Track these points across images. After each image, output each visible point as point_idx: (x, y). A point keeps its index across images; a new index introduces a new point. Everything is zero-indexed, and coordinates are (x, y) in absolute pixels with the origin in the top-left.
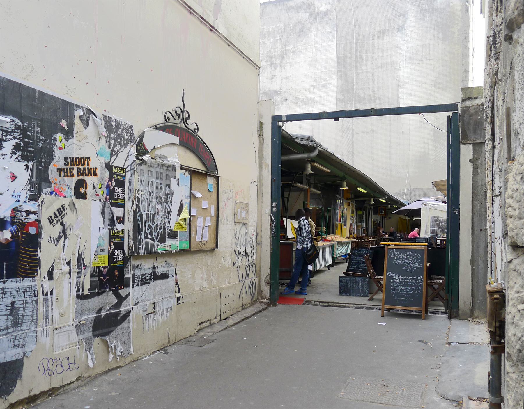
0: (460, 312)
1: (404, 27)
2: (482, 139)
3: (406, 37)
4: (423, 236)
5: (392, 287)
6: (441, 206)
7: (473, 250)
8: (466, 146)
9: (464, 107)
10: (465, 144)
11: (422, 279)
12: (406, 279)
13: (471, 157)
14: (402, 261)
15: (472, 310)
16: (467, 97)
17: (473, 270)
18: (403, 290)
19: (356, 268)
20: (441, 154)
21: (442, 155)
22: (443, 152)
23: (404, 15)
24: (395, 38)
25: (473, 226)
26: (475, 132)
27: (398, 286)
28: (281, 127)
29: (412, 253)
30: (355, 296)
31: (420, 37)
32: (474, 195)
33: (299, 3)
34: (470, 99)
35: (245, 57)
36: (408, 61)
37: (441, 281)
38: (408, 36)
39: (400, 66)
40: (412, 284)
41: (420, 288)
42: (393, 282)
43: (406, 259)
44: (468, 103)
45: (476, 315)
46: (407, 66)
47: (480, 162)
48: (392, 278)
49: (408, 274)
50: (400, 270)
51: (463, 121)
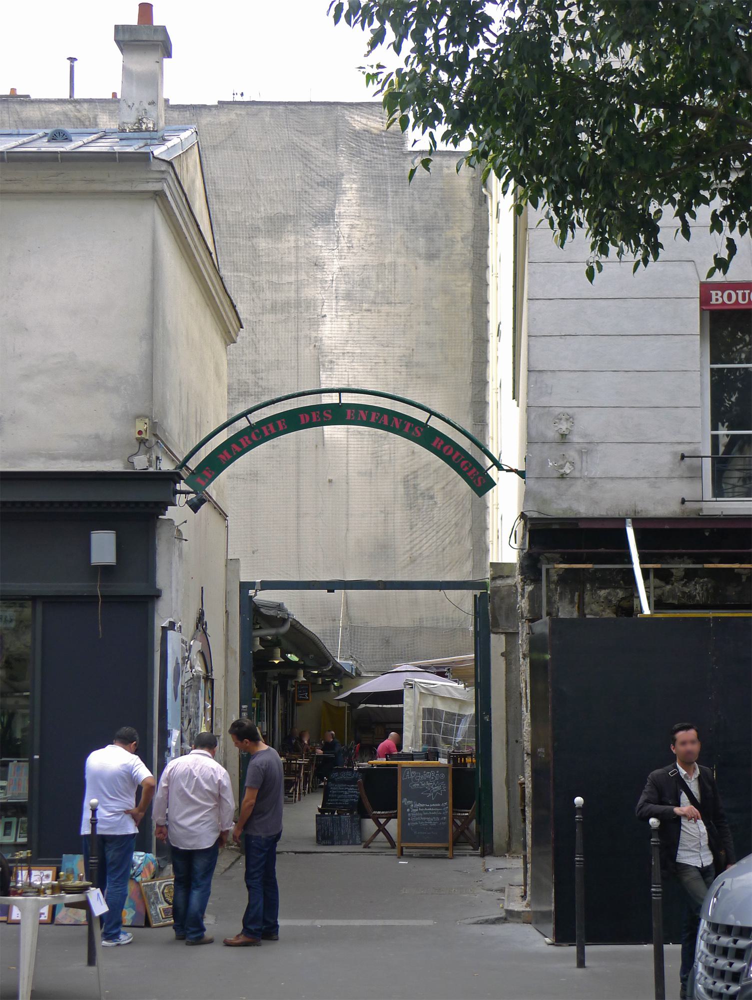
0: (495, 847)
1: (333, 215)
2: (515, 628)
3: (338, 240)
4: (407, 748)
5: (409, 819)
6: (443, 687)
7: (507, 767)
8: (497, 636)
9: (495, 587)
10: (496, 633)
11: (446, 806)
12: (427, 807)
13: (504, 650)
14: (420, 785)
15: (509, 844)
16: (499, 574)
17: (509, 791)
18: (424, 821)
19: (339, 802)
20: (424, 542)
21: (427, 545)
22: (429, 537)
23: (333, 184)
24: (311, 239)
25: (507, 737)
26: (507, 618)
27: (417, 817)
28: (251, 597)
29: (432, 773)
30: (341, 844)
31: (372, 244)
32: (508, 698)
33: (52, 114)
34: (501, 577)
35: (216, 507)
36: (342, 303)
37: (467, 814)
38: (342, 238)
39: (324, 314)
40: (435, 813)
41: (445, 818)
42: (410, 812)
43: (425, 781)
44: (499, 582)
45: (513, 849)
46: (340, 314)
47: (513, 656)
48: (409, 806)
49: (428, 801)
50: (419, 796)
51: (493, 604)
